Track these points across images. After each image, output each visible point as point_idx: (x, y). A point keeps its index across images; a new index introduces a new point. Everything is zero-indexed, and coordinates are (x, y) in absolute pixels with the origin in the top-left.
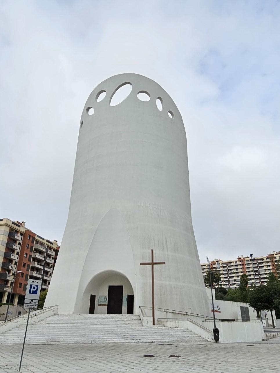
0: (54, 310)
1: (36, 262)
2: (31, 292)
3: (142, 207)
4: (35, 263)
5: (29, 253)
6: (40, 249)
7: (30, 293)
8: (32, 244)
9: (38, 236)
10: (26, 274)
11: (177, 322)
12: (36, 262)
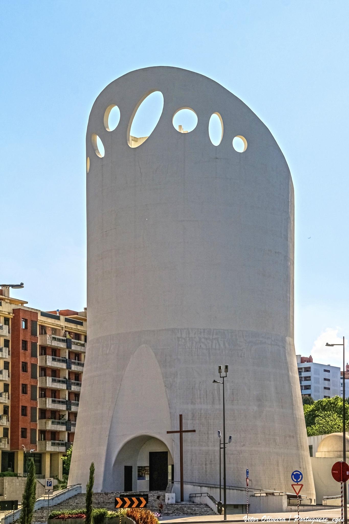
0: (77, 489)
1: (48, 378)
2: (48, 485)
3: (183, 341)
4: (46, 380)
5: (30, 361)
6: (53, 344)
7: (47, 486)
8: (33, 337)
9: (43, 314)
10: (32, 408)
11: (267, 497)
12: (48, 378)
